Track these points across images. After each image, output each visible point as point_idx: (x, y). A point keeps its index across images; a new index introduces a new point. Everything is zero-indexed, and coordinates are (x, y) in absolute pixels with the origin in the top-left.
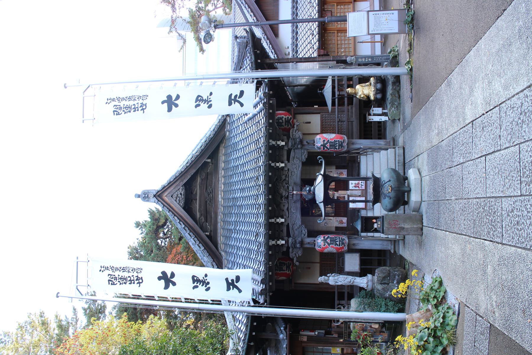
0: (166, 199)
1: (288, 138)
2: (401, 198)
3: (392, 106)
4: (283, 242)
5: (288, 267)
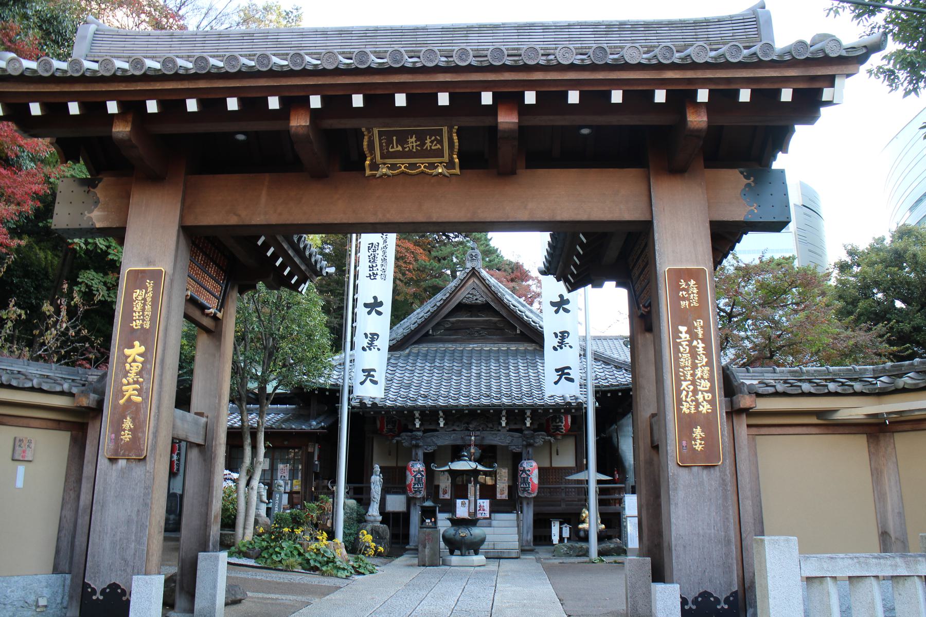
0: (471, 282)
1: (535, 430)
2: (456, 546)
3: (569, 548)
4: (418, 426)
5: (391, 430)
